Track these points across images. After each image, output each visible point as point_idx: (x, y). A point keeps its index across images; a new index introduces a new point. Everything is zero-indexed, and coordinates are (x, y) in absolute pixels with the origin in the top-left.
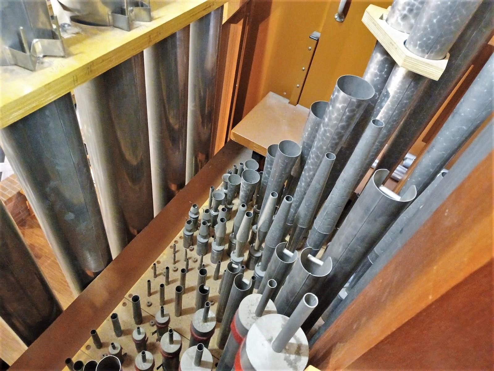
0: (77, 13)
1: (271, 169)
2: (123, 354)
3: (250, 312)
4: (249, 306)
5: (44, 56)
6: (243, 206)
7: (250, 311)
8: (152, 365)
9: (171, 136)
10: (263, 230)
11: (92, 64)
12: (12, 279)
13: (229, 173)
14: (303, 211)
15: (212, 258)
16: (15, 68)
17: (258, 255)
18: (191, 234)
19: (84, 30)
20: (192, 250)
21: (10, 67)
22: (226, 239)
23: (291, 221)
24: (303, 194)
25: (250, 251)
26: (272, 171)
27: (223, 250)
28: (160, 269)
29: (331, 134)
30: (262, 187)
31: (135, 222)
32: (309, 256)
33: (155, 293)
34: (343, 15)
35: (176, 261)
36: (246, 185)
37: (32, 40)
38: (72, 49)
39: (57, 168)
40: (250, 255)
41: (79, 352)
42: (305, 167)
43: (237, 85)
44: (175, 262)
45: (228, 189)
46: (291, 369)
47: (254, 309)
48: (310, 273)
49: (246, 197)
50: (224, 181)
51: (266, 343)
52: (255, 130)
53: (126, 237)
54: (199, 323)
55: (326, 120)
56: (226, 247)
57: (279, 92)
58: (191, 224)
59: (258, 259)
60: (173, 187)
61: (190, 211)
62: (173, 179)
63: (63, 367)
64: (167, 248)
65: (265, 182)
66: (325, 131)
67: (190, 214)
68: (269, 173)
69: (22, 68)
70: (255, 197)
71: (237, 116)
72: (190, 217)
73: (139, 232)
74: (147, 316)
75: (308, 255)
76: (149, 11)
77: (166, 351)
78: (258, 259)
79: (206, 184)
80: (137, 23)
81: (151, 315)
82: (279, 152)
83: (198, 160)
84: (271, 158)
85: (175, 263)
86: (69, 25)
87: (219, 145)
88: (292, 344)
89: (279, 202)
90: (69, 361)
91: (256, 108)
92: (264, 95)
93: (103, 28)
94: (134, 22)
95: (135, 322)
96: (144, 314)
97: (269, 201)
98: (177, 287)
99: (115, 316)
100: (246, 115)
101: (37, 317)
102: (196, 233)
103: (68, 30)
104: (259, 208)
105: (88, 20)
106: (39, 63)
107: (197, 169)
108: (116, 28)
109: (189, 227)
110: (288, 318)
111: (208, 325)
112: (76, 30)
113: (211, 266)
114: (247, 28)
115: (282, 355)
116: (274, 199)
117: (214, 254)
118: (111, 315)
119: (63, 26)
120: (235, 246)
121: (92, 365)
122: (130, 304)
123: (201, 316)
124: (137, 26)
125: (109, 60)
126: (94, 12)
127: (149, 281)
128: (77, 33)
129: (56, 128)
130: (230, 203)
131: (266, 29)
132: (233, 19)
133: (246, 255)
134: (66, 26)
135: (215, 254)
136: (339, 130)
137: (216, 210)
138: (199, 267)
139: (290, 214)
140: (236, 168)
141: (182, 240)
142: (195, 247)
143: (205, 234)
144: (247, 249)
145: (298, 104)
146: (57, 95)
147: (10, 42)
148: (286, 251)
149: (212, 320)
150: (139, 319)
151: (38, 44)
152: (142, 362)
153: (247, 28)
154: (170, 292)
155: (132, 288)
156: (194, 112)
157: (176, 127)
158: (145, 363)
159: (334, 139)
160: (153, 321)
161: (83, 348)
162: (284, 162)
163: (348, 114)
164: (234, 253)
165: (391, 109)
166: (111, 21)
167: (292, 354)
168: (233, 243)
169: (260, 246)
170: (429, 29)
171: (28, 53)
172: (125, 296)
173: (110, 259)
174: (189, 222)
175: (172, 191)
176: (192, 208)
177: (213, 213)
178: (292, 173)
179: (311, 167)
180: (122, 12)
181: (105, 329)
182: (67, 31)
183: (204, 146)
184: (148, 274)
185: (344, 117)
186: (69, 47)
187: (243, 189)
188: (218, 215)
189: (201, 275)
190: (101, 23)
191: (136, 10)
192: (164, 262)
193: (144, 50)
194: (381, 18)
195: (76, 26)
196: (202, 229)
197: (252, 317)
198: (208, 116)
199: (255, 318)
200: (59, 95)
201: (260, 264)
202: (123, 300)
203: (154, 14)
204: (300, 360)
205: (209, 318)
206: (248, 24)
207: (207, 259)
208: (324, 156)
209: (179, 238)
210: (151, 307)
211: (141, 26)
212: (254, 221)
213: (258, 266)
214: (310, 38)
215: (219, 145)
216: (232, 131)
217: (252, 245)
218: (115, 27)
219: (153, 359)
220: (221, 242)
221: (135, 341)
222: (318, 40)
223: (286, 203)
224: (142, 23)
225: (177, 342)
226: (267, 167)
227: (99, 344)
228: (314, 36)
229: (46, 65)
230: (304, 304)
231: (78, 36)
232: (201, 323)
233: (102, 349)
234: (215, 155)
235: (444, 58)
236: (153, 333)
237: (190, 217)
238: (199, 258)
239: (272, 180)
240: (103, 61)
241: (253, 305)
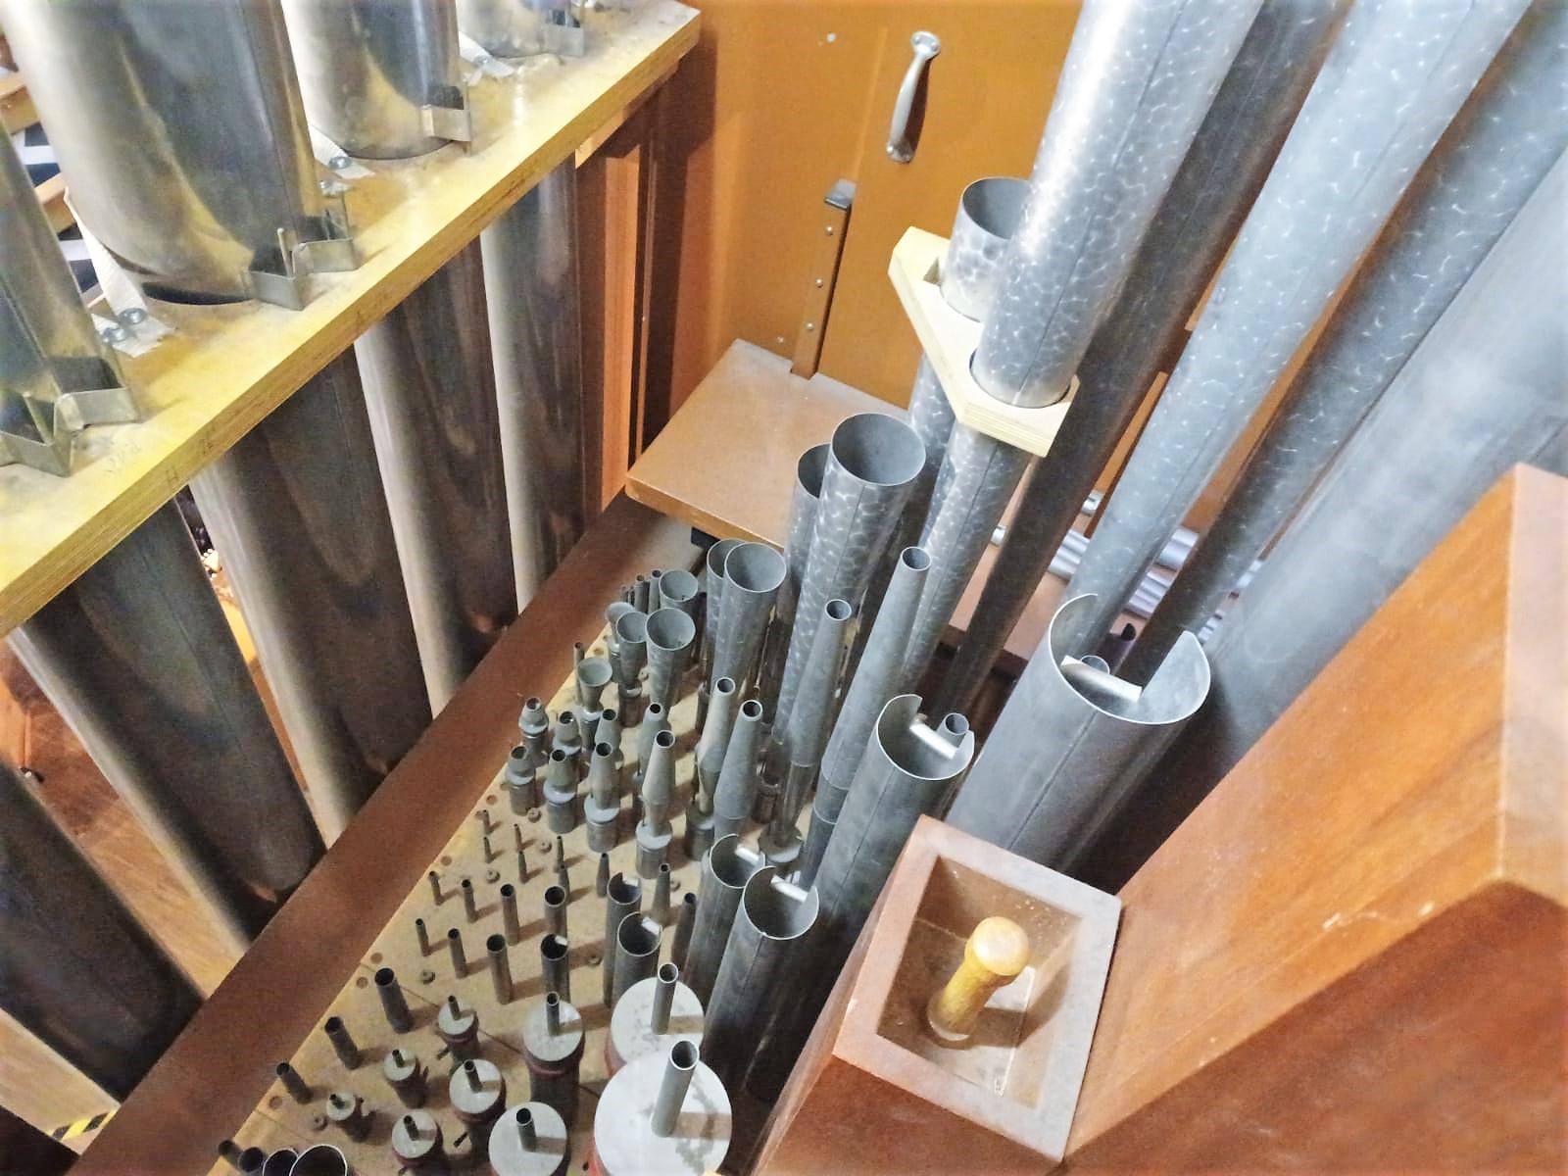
0: (156, 280)
2: (365, 1113)
7: (639, 1021)
8: (435, 1144)
11: (212, 426)
15: (591, 838)
17: (707, 825)
19: (182, 325)
20: (536, 820)
22: (622, 783)
27: (617, 818)
29: (836, 552)
31: (379, 735)
32: (776, 880)
34: (909, 144)
35: (492, 852)
41: (254, 1115)
43: (644, 319)
46: (690, 1171)
47: (648, 1016)
53: (359, 783)
54: (540, 1038)
55: (822, 520)
57: (762, 338)
58: (525, 757)
63: (210, 1165)
64: (467, 819)
66: (823, 544)
71: (653, 416)
73: (392, 765)
77: (464, 1109)
79: (578, 613)
80: (321, 277)
86: (143, 315)
88: (692, 1116)
90: (227, 1148)
92: (726, 345)
94: (311, 275)
99: (334, 1025)
100: (677, 410)
101: (134, 1018)
107: (548, 562)
111: (561, 1042)
113: (589, 859)
115: (672, 1142)
118: (324, 1020)
119: (124, 320)
121: (283, 1158)
126: (200, 265)
127: (419, 922)
128: (166, 337)
131: (708, 171)
134: (135, 317)
136: (855, 546)
145: (816, 370)
146: (129, 524)
150: (404, 1018)
152: (410, 1140)
155: (377, 940)
159: (847, 564)
161: (262, 1106)
163: (865, 514)
164: (643, 825)
165: (964, 503)
167: (695, 1137)
170: (1008, 349)
172: (362, 961)
174: (518, 753)
176: (526, 711)
179: (808, 619)
182: (139, 335)
184: (418, 900)
185: (858, 521)
186: (148, 383)
189: (553, 904)
194: (934, 277)
197: (645, 1038)
199: (651, 1037)
200: (133, 526)
204: (711, 1148)
205: (564, 1024)
207: (577, 841)
208: (819, 614)
209: (498, 788)
210: (432, 984)
211: (332, 287)
214: (826, 205)
219: (436, 1128)
222: (849, 211)
227: (304, 1093)
228: (839, 197)
229: (94, 450)
233: (311, 1105)
235: (1062, 399)
240: (238, 412)
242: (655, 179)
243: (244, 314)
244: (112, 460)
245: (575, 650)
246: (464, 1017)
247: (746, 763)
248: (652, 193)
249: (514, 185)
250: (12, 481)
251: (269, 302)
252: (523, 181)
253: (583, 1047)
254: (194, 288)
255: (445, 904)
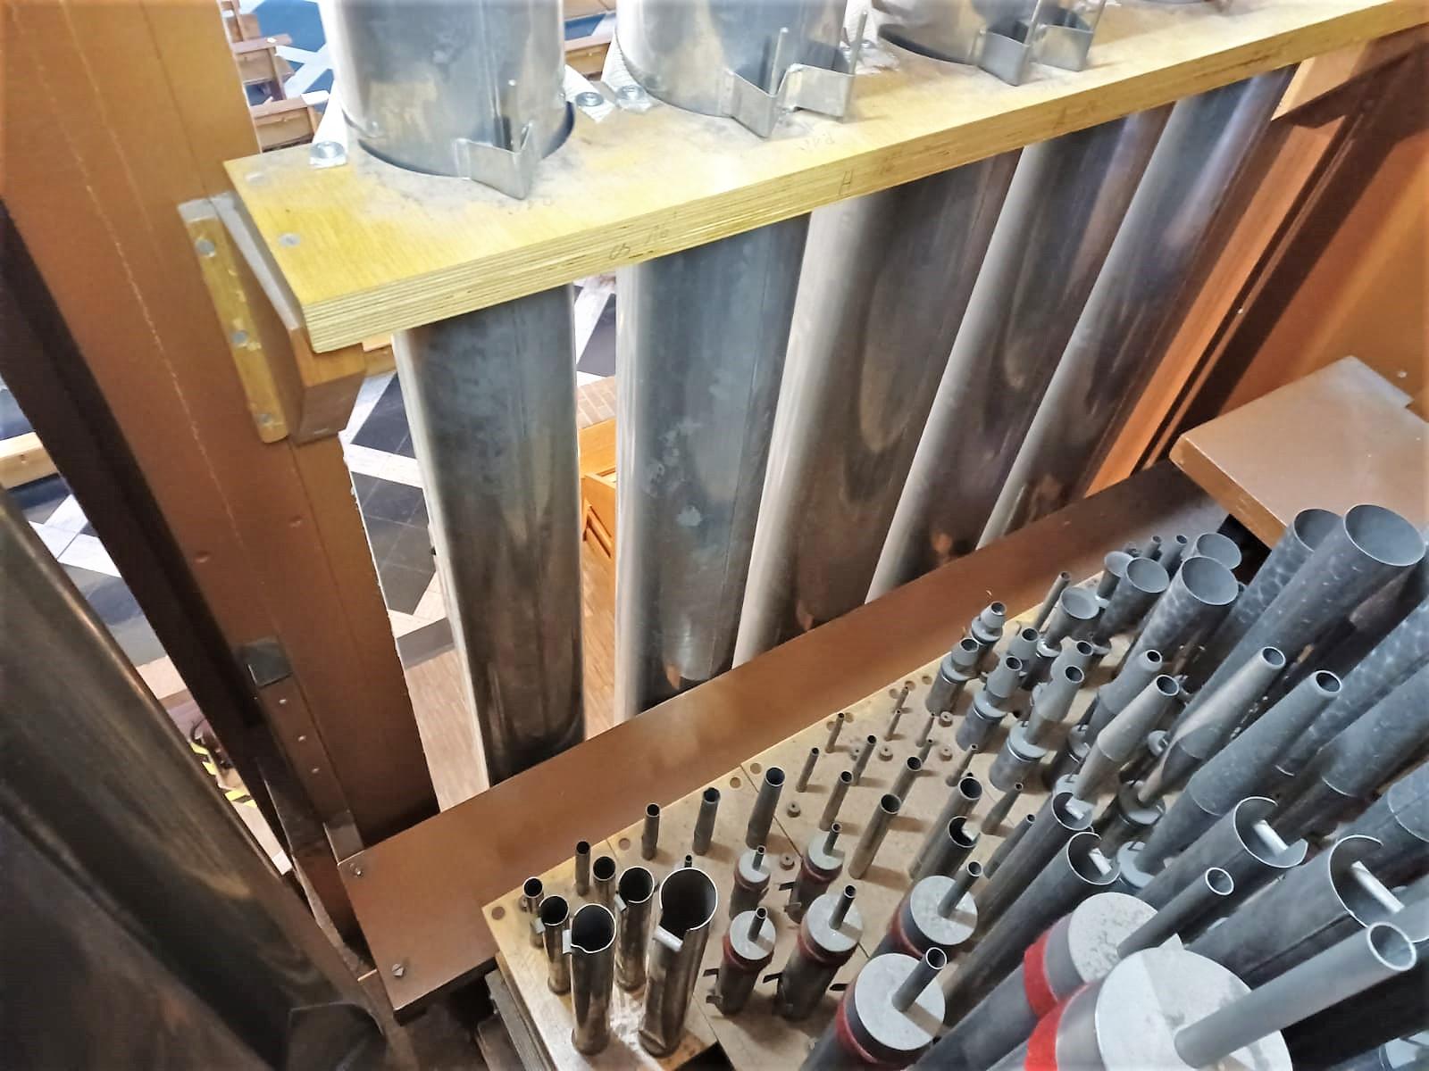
0: (899, 20)
1: (1285, 580)
3: (1103, 936)
4: (1105, 921)
5: (799, 109)
6: (1153, 657)
9: (994, 405)
10: (1191, 750)
12: (530, 614)
13: (1130, 552)
14: (1359, 739)
15: (997, 768)
16: (730, 124)
18: (960, 677)
19: (905, 65)
20: (945, 724)
21: (719, 121)
23: (1293, 761)
24: (1374, 692)
25: (1120, 796)
26: (1285, 591)
28: (852, 735)
30: (1229, 628)
31: (816, 595)
33: (817, 789)
35: (895, 732)
36: (1183, 601)
37: (789, 65)
38: (863, 105)
39: (713, 390)
40: (1116, 809)
42: (1419, 608)
44: (891, 736)
45: (1116, 596)
48: (1352, 913)
49: (1168, 635)
50: (1107, 572)
51: (1161, 1023)
52: (1259, 456)
53: (783, 624)
54: (927, 909)
56: (1049, 757)
57: (1383, 363)
59: (1138, 831)
60: (942, 543)
61: (977, 618)
62: (951, 522)
65: (1246, 616)
67: (975, 625)
68: (1271, 592)
69: (743, 128)
70: (1201, 646)
71: (1207, 401)
72: (973, 632)
73: (817, 623)
74: (779, 837)
75: (1355, 862)
76: (1085, 42)
77: (816, 938)
78: (1138, 831)
79: (1029, 573)
80: (1043, 68)
81: (789, 839)
82: (1340, 534)
83: (1034, 497)
84: (1298, 547)
85: (890, 740)
86: (872, 46)
87: (1116, 468)
89: (1275, 687)
91: (1284, 393)
93: (952, 65)
94: (1034, 64)
95: (745, 836)
96: (774, 830)
97: (1244, 674)
98: (885, 797)
99: (712, 795)
102: (974, 685)
103: (867, 56)
104: (1192, 687)
105: (916, 41)
106: (781, 122)
108: (982, 72)
109: (966, 657)
110: (1247, 989)
111: (948, 927)
112: (887, 59)
114: (1348, 145)
116: (1269, 669)
117: (1006, 760)
118: (706, 787)
120: (1081, 766)
122: (760, 779)
123: (938, 895)
124: (1039, 76)
125: (940, 150)
126: (943, 19)
127: (815, 751)
128: (886, 68)
129: (751, 287)
130: (1103, 640)
132: (1310, 114)
133: (1105, 801)
135: (1011, 761)
137: (1054, 643)
138: (950, 777)
139: (1302, 739)
140: (1158, 546)
141: (928, 688)
142: (958, 721)
143: (1001, 695)
144: (1108, 791)
147: (741, 61)
148: (1265, 830)
149: (964, 918)
150: (759, 832)
151: (799, 79)
153: (1348, 145)
154: (860, 807)
156: (1081, 353)
157: (1017, 382)
158: (751, 943)
160: (790, 857)
162: (1349, 566)
166: (978, 53)
168: (1074, 754)
169: (1156, 797)
171: (772, 94)
172: (742, 764)
173: (726, 666)
174: (968, 644)
175: (935, 553)
176: (987, 612)
177: (1043, 648)
178: (1354, 617)
180: (1018, 32)
181: (679, 814)
182: (865, 59)
183: (1069, 461)
184: (815, 734)
186: (858, 97)
187: (1167, 608)
188: (1054, 658)
190: (949, 54)
191: (1054, 33)
192: (864, 721)
193: (1025, 147)
195: (887, 50)
196: (1000, 676)
197: (1107, 956)
198: (1115, 381)
201: (1140, 845)
202: (735, 771)
203: (1096, 52)
206: (1354, 137)
207: (982, 767)
209: (919, 678)
210: (946, 762)
212: (1170, 712)
213: (1130, 849)
215: (1116, 468)
216: (1186, 437)
217: (1132, 782)
218: (983, 69)
220: (1048, 733)
221: (738, 876)
223: (1311, 689)
224: (1056, 72)
225: (851, 932)
226: (1272, 572)
229: (795, 130)
230: (1368, 948)
231: (887, 74)
232: (933, 914)
234: (1090, 497)
236: (784, 887)
237: (973, 632)
238: (959, 754)
239: (1280, 612)
241: (1120, 925)
242: (1339, 163)
243: (963, 73)
244: (807, 142)
245: (1060, 576)
246: (835, 856)
247: (1276, 748)
248: (1333, 168)
249: (1258, 57)
250: (722, 129)
251: (986, 71)
252: (1266, 57)
253: (875, 952)
254: (925, 43)
255: (832, 754)
